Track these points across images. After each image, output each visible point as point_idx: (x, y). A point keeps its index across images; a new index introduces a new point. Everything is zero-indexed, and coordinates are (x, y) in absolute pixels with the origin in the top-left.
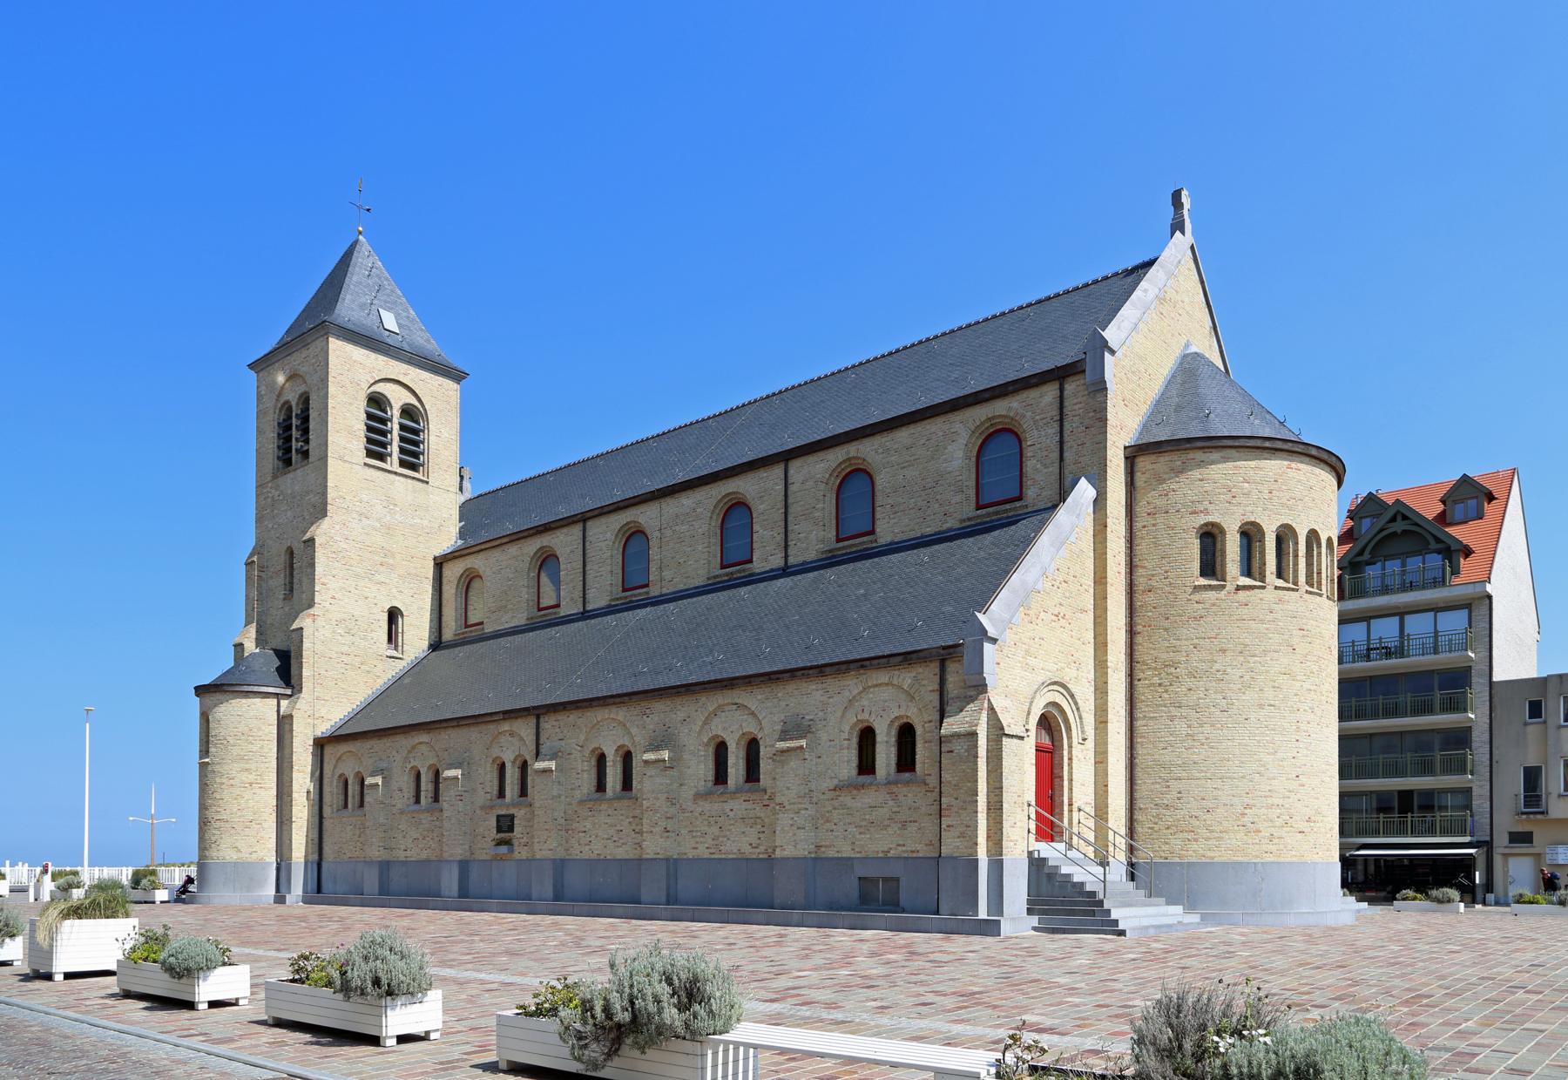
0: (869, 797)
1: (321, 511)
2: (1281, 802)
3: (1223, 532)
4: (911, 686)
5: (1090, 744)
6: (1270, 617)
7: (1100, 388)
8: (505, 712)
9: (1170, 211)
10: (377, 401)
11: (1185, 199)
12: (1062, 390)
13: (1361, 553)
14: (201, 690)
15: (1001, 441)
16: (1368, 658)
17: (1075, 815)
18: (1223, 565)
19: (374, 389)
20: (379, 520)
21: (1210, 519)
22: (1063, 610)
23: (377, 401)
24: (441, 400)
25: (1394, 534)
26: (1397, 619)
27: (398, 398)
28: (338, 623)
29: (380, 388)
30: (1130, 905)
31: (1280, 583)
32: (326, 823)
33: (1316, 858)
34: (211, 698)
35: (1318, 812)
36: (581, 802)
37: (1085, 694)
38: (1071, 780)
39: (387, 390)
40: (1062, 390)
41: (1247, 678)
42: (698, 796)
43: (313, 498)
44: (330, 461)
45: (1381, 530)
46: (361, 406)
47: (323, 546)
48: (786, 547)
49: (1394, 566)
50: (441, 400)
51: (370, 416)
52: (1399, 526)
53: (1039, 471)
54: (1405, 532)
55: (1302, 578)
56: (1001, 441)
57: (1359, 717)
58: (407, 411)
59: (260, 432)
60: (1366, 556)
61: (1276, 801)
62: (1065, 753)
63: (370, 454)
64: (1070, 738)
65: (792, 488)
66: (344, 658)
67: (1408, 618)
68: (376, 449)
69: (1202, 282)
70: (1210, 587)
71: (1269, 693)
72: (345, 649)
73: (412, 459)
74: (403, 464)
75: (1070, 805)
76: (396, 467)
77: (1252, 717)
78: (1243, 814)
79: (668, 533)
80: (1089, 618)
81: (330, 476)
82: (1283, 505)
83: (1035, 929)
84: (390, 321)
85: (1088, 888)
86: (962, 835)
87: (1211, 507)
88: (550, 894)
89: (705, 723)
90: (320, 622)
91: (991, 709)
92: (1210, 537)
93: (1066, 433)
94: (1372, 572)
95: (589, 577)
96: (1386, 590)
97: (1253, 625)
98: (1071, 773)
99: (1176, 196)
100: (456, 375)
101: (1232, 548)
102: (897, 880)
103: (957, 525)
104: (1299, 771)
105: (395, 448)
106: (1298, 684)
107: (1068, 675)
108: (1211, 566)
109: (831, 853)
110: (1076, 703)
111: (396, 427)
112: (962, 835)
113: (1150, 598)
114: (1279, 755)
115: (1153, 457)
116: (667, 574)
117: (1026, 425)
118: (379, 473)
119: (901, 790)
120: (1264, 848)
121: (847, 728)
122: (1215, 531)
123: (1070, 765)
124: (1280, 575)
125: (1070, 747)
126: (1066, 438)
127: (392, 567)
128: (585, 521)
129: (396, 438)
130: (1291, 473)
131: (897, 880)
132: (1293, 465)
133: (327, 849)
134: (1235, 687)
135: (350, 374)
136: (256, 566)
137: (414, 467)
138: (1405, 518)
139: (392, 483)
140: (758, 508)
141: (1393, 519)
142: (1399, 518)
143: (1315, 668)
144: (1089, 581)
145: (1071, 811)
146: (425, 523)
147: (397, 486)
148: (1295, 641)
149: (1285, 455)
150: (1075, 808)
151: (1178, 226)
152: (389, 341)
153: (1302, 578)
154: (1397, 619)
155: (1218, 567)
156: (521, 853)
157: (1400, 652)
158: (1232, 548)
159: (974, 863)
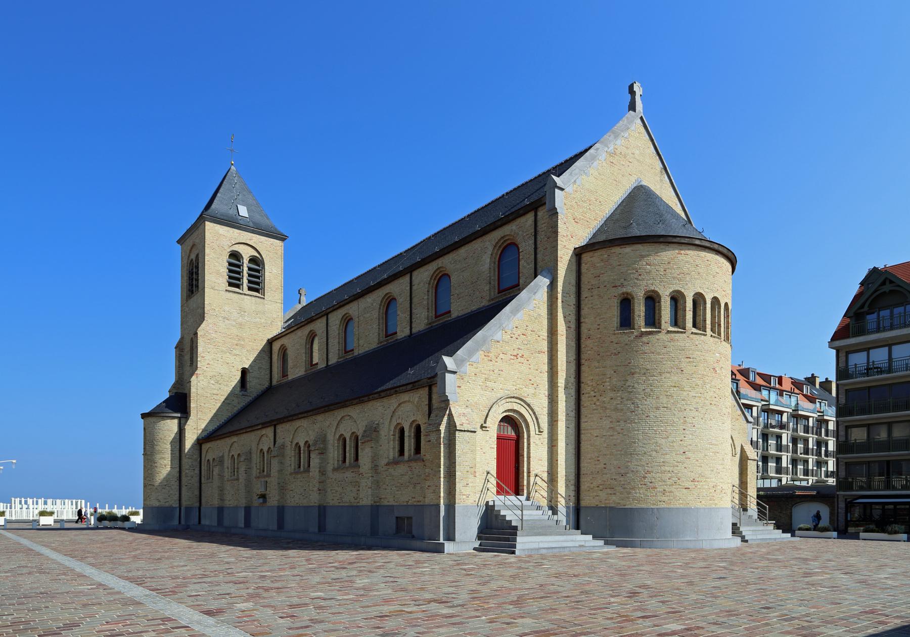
0: (402, 469)
1: (202, 318)
2: (671, 469)
3: (659, 296)
4: (418, 402)
5: (545, 434)
6: (665, 350)
7: (554, 213)
8: (263, 424)
9: (628, 97)
10: (235, 255)
11: (637, 88)
12: (536, 216)
13: (862, 306)
14: (144, 416)
15: (508, 248)
16: (867, 375)
17: (532, 479)
18: (660, 320)
19: (232, 249)
20: (234, 320)
21: (624, 290)
22: (520, 353)
23: (235, 255)
24: (272, 251)
25: (885, 292)
26: (886, 349)
27: (246, 253)
28: (211, 377)
29: (237, 248)
30: (551, 535)
31: (694, 330)
32: (203, 486)
33: (699, 505)
34: (151, 420)
35: (701, 475)
36: (291, 474)
37: (541, 405)
38: (529, 457)
39: (241, 249)
40: (536, 216)
41: (648, 390)
42: (334, 470)
43: (200, 311)
44: (206, 290)
45: (876, 291)
46: (224, 260)
47: (203, 336)
48: (411, 322)
49: (885, 313)
50: (272, 251)
51: (230, 264)
52: (887, 288)
53: (526, 265)
54: (891, 291)
55: (709, 326)
56: (508, 248)
57: (851, 414)
58: (253, 260)
59: (182, 277)
60: (866, 308)
61: (667, 469)
62: (525, 441)
63: (230, 284)
64: (528, 431)
65: (414, 288)
66: (215, 397)
67: (894, 348)
68: (234, 281)
69: (652, 140)
70: (678, 332)
71: (664, 400)
72: (215, 392)
73: (257, 285)
74: (250, 289)
75: (529, 472)
76: (246, 290)
77: (651, 415)
78: (645, 478)
79: (362, 318)
80: (545, 358)
81: (206, 298)
82: (674, 278)
83: (475, 549)
84: (243, 211)
85: (514, 524)
86: (434, 492)
87: (626, 283)
88: (316, 530)
89: (337, 427)
90: (201, 377)
91: (450, 415)
92: (626, 303)
93: (538, 242)
94: (871, 318)
95: (330, 346)
96: (878, 330)
97: (652, 356)
98: (529, 453)
99: (631, 88)
100: (282, 238)
101: (640, 310)
102: (411, 518)
103: (487, 304)
104: (686, 449)
105: (245, 281)
106: (685, 393)
107: (527, 392)
108: (626, 321)
109: (386, 503)
110: (532, 410)
111: (246, 269)
112: (434, 492)
113: (589, 342)
114: (670, 439)
115: (591, 254)
116: (361, 342)
117: (518, 240)
118: (235, 295)
119: (413, 464)
120: (659, 498)
121: (392, 428)
122: (629, 297)
123: (529, 448)
124: (694, 326)
125: (529, 436)
126: (538, 246)
127: (243, 346)
128: (327, 315)
129: (247, 275)
130: (680, 257)
131: (411, 518)
132: (683, 252)
133: (203, 501)
134: (640, 397)
135: (219, 241)
136: (179, 347)
137: (257, 290)
138: (891, 282)
139: (243, 300)
140: (400, 300)
141: (884, 283)
142: (887, 283)
143: (700, 382)
144: (544, 333)
145: (529, 476)
146: (263, 321)
147: (247, 301)
148: (683, 365)
149: (676, 246)
150: (532, 474)
151: (632, 107)
152: (241, 222)
153: (709, 326)
154: (886, 349)
155: (657, 321)
156: (268, 504)
157: (890, 370)
158: (640, 310)
159: (438, 506)
